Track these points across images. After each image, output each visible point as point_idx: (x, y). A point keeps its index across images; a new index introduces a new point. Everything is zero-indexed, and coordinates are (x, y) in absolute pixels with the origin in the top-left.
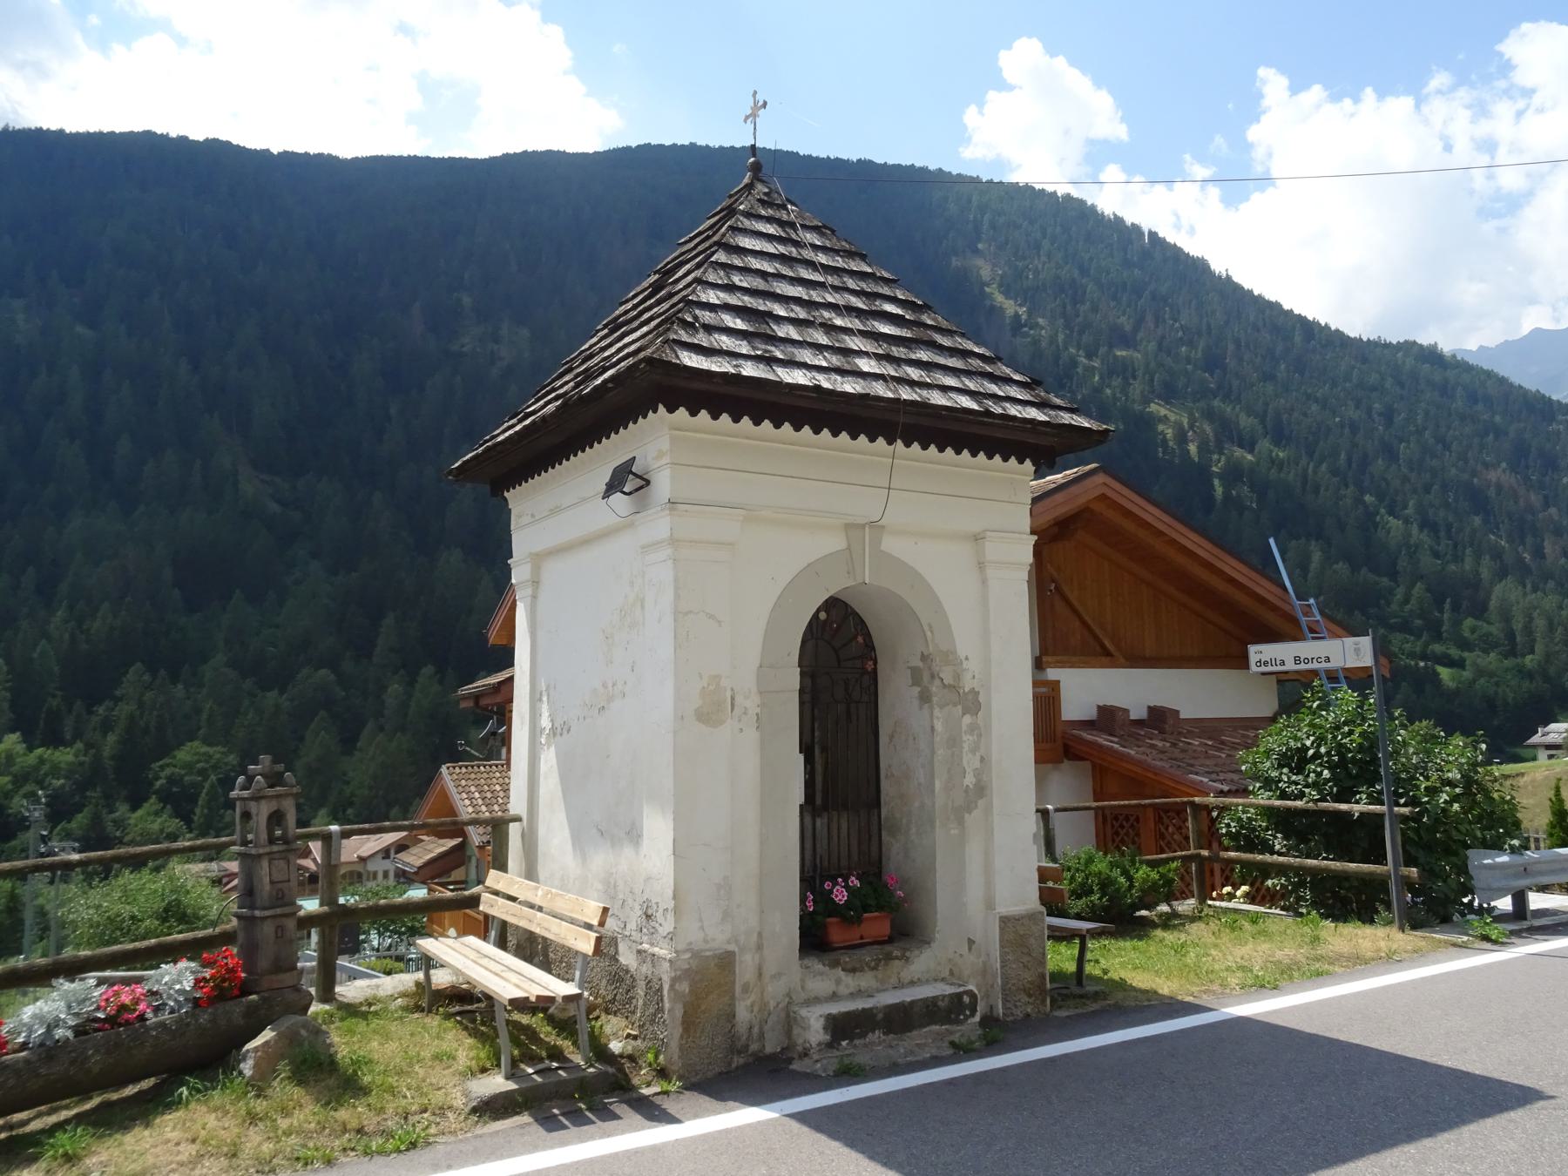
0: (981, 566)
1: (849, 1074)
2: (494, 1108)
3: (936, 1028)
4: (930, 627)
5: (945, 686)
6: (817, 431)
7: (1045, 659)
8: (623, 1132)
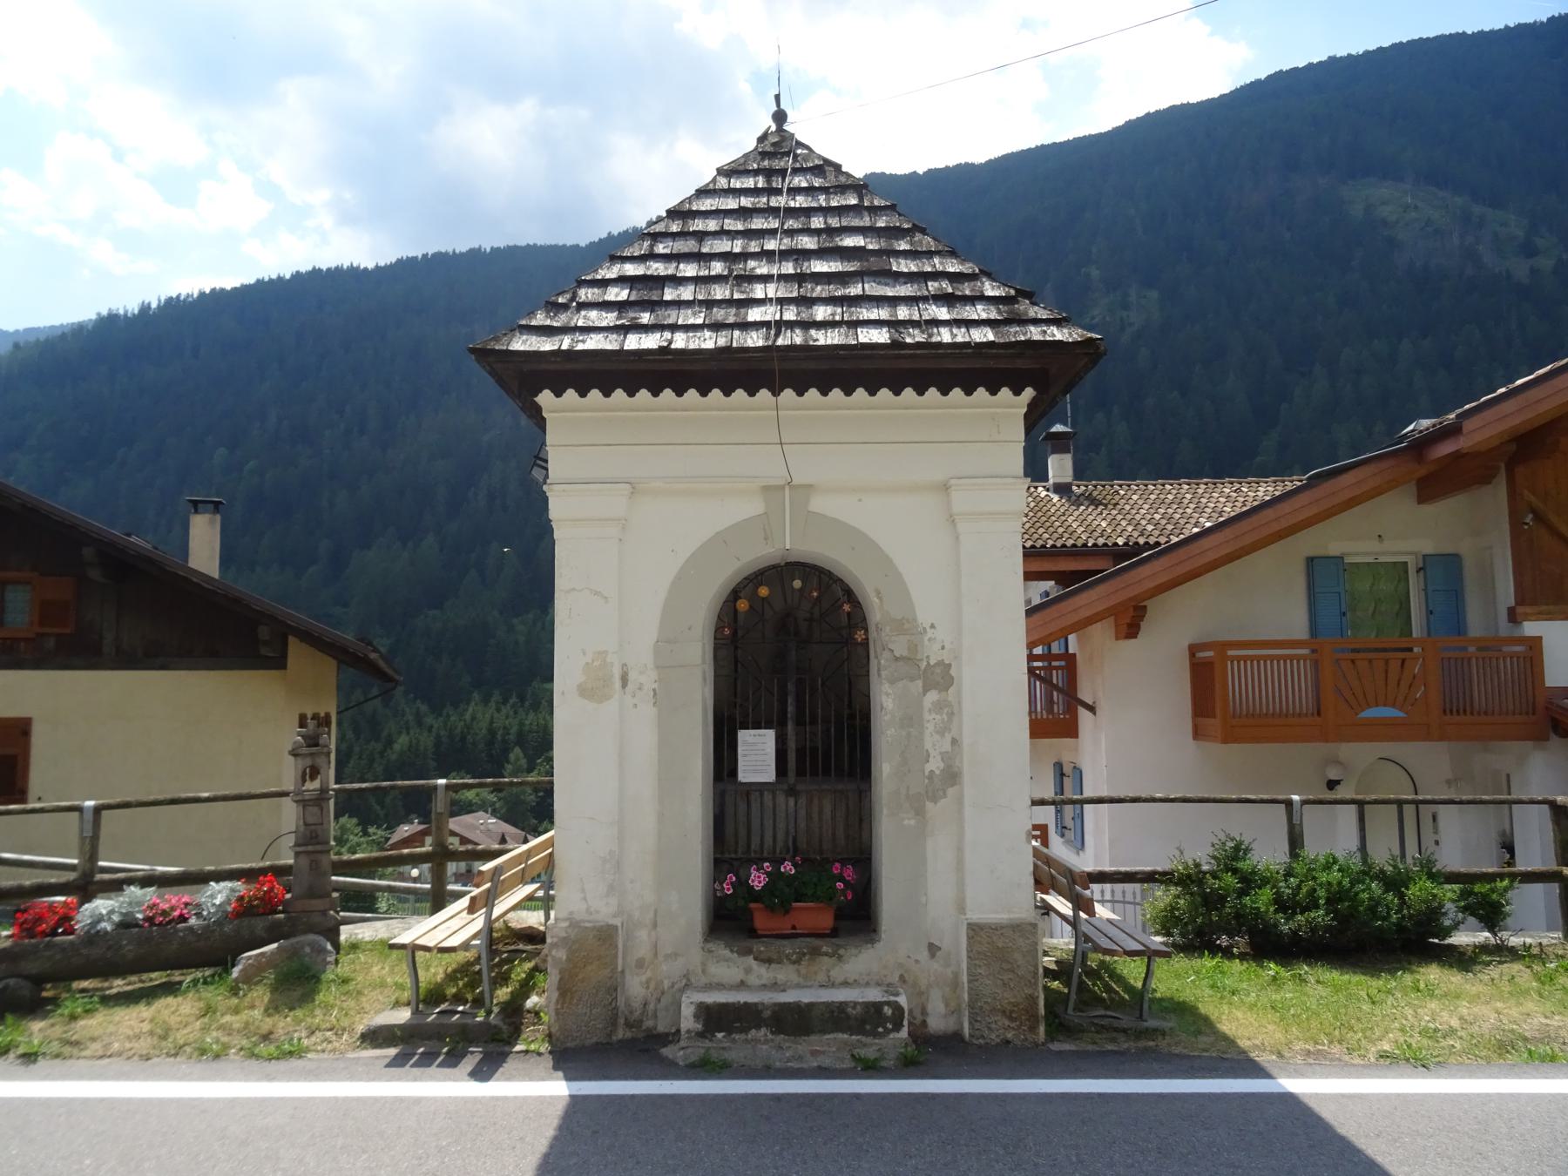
0: (952, 520)
1: (705, 1068)
2: (375, 1037)
3: (840, 1036)
4: (878, 593)
5: (897, 659)
7: (1520, 610)
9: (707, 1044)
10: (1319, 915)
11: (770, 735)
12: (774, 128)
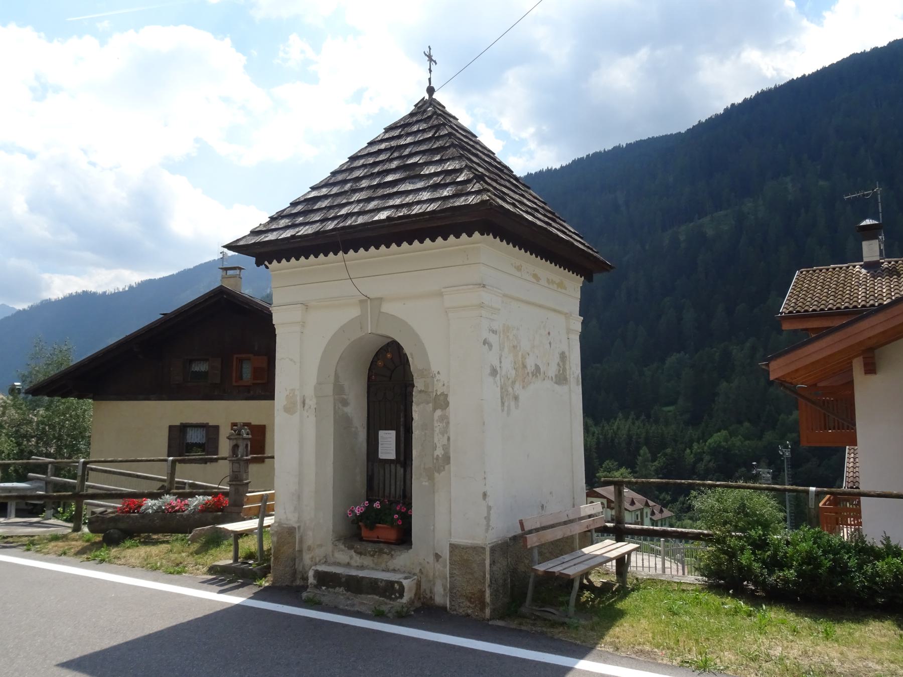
4: (411, 354)
6: (410, 243)
8: (211, 591)
9: (317, 591)
10: (791, 574)
11: (393, 433)
12: (427, 97)
